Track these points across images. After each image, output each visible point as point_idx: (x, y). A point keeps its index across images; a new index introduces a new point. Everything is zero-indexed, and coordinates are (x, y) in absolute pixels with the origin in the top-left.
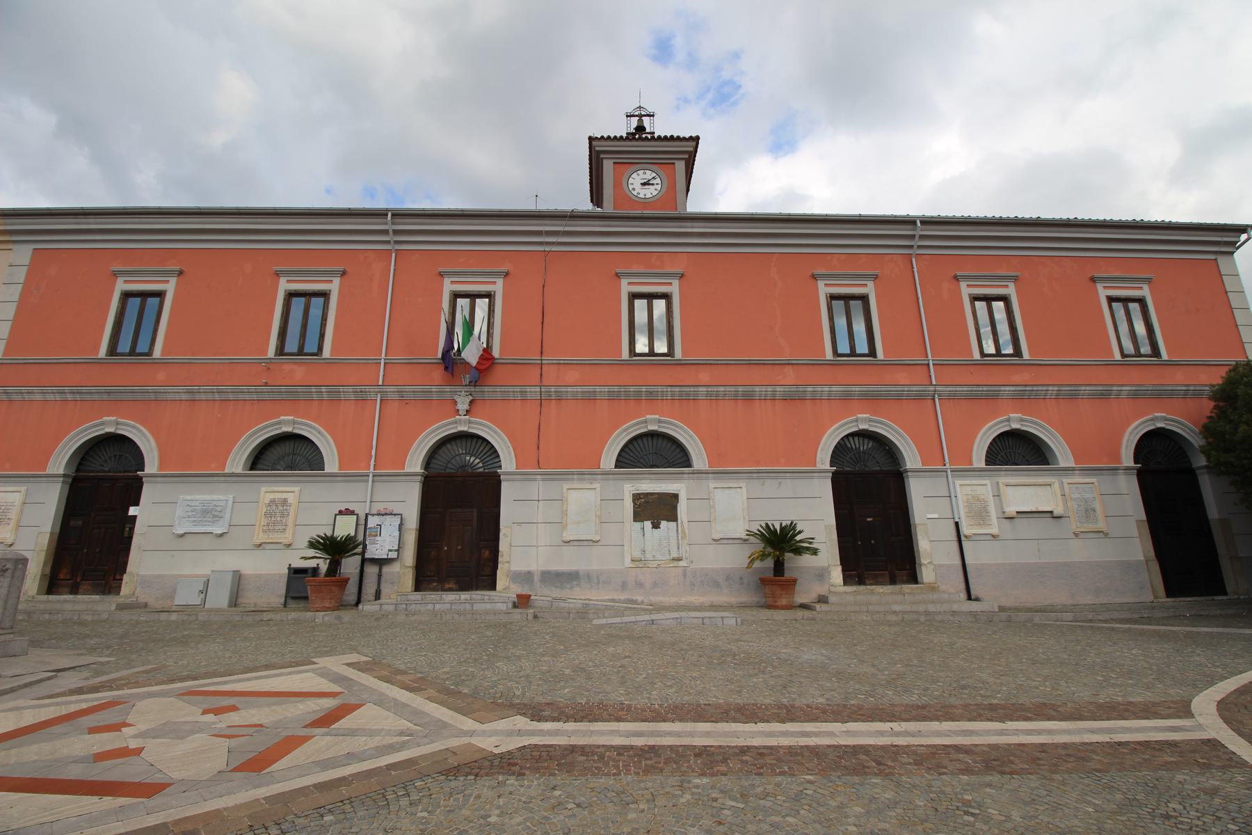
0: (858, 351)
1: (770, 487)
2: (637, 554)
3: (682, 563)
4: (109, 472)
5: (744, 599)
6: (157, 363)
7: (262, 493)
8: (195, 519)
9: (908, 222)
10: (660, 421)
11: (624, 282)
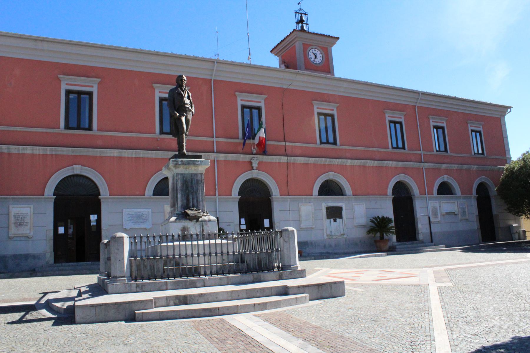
0: (441, 150)
2: (329, 233)
3: (345, 236)
8: (134, 221)
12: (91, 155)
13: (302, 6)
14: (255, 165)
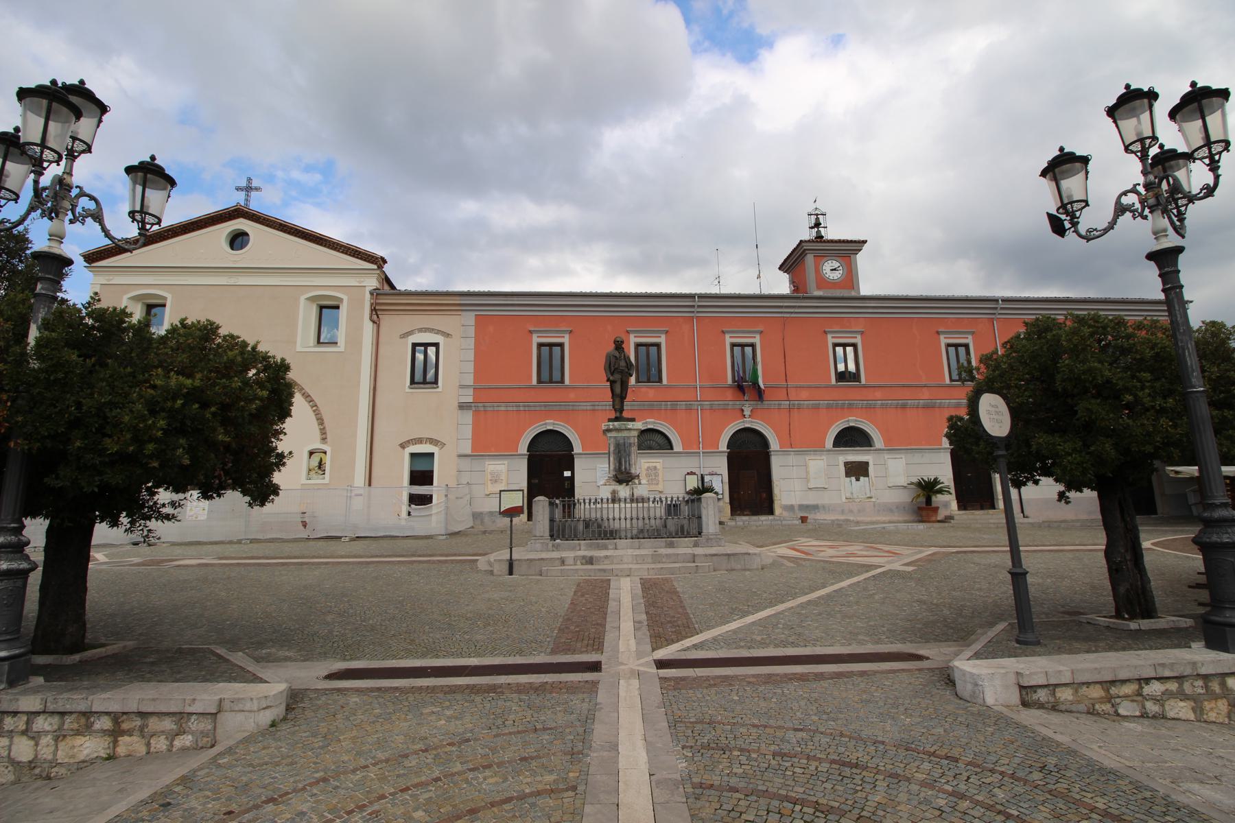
1: (917, 458)
2: (848, 495)
3: (873, 500)
4: (547, 451)
5: (906, 518)
6: (567, 387)
7: (486, 465)
9: (691, 297)
10: (554, 424)
11: (942, 337)
12: (42, 663)
13: (818, 205)
14: (747, 413)
